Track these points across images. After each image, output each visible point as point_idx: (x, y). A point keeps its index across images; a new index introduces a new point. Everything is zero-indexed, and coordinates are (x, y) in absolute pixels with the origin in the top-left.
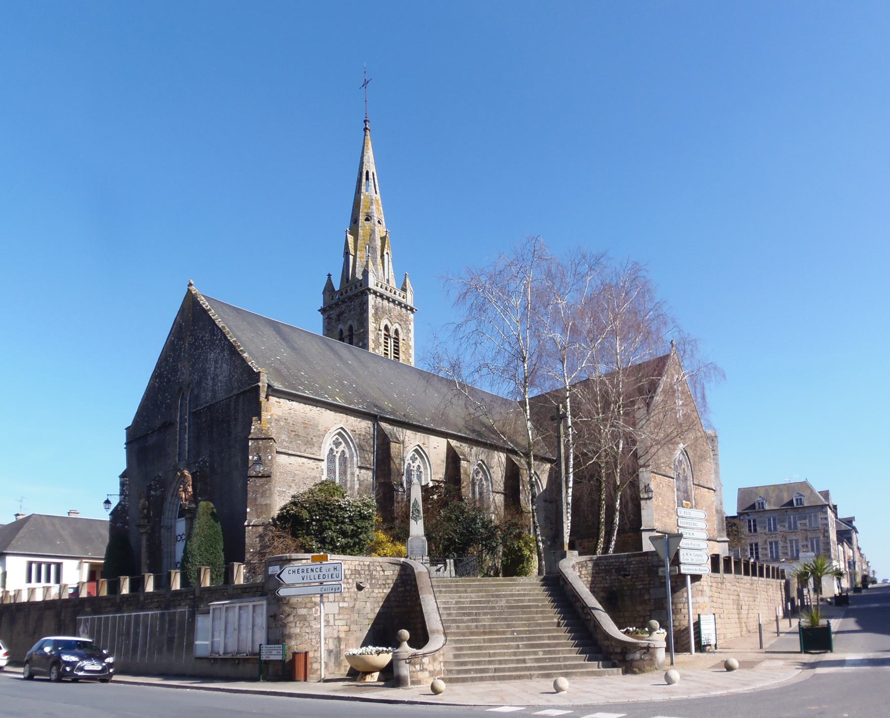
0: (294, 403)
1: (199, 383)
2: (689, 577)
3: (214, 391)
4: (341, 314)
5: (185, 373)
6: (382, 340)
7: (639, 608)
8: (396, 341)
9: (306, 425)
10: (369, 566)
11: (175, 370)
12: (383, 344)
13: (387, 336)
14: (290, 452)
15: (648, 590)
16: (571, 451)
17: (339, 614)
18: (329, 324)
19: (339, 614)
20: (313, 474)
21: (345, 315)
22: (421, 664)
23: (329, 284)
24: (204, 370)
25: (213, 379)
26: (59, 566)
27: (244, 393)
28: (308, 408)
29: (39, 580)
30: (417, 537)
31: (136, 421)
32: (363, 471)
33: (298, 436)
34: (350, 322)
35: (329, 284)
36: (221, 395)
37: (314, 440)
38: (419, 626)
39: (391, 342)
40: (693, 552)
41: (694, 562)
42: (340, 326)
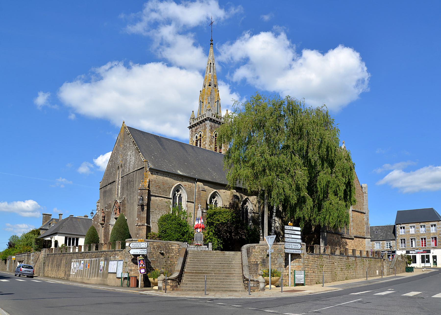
1: (124, 164)
2: (290, 255)
6: (214, 141)
9: (163, 183)
10: (165, 244)
11: (117, 159)
14: (156, 195)
18: (192, 133)
23: (193, 115)
40: (292, 244)
41: (293, 248)
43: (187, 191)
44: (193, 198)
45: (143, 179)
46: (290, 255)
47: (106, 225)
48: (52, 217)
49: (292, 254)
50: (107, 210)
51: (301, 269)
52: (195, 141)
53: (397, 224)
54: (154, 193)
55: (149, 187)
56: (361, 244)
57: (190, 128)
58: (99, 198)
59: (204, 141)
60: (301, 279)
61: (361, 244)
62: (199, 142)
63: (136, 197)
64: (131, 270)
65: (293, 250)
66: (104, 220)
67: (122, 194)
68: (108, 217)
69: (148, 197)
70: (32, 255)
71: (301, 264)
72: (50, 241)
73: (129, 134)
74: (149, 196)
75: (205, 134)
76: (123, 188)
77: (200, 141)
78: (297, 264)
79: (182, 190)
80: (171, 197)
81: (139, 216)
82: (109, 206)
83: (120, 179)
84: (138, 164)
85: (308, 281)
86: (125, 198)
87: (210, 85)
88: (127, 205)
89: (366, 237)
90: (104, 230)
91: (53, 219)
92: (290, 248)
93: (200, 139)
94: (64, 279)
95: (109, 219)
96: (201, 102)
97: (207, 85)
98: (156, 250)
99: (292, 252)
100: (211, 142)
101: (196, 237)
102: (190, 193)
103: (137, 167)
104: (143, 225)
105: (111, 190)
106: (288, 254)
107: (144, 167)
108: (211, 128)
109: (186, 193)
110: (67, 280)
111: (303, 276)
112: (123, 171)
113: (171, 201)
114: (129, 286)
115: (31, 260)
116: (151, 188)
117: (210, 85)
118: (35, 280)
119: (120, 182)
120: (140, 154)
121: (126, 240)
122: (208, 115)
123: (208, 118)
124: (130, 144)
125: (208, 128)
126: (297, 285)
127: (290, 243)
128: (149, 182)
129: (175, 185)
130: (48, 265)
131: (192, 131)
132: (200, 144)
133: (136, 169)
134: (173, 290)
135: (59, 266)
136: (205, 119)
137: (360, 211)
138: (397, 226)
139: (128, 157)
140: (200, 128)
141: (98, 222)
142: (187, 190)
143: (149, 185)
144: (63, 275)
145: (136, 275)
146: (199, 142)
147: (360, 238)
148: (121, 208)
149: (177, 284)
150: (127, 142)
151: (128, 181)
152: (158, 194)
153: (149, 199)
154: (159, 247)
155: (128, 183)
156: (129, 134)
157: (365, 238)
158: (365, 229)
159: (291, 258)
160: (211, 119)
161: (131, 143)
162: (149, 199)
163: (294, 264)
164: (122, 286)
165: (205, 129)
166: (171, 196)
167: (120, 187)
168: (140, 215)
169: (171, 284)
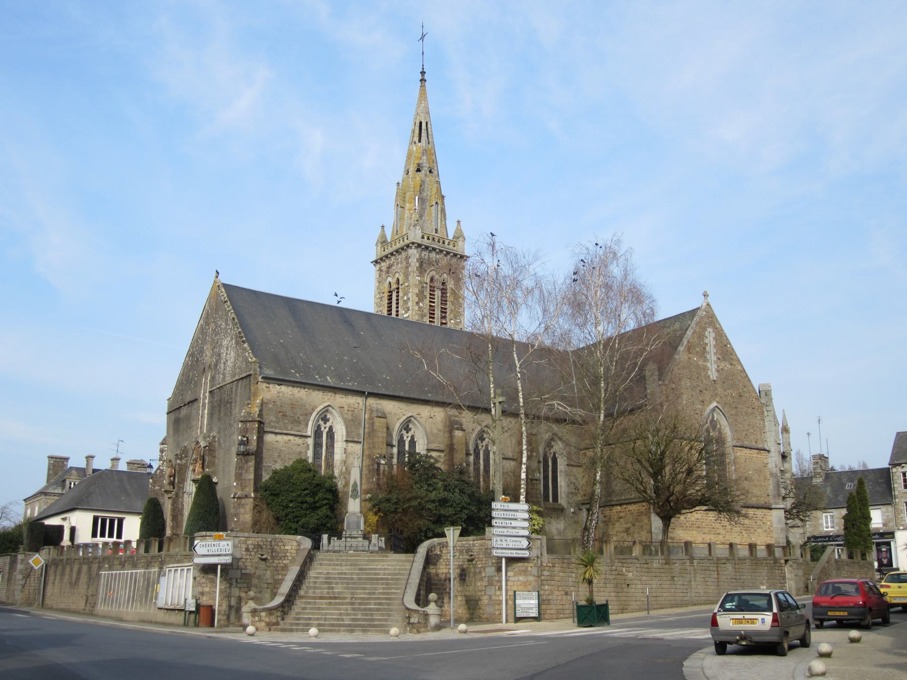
0: (283, 387)
1: (216, 365)
2: (504, 560)
3: (224, 374)
4: (389, 267)
5: (208, 357)
6: (427, 293)
7: (479, 584)
8: (444, 291)
9: (293, 406)
10: (271, 542)
11: (201, 351)
12: (428, 296)
13: (432, 289)
14: (277, 431)
15: (484, 568)
16: (524, 429)
17: (241, 578)
18: (380, 276)
19: (241, 578)
20: (298, 450)
21: (393, 268)
22: (260, 617)
23: (383, 235)
24: (219, 355)
25: (224, 363)
26: (121, 521)
27: (242, 379)
28: (296, 390)
29: (111, 535)
30: (354, 514)
31: (174, 394)
32: (350, 445)
33: (285, 415)
34: (397, 275)
35: (383, 235)
36: (229, 379)
37: (301, 418)
38: (869, 620)
39: (438, 293)
40: (509, 539)
41: (511, 546)
42: (390, 279)
43: (345, 420)
44: (359, 435)
45: (249, 399)
46: (504, 560)
47: (177, 495)
48: (70, 464)
49: (507, 558)
50: (179, 461)
51: (530, 588)
52: (386, 294)
53: (895, 465)
54: (272, 427)
55: (260, 415)
56: (759, 523)
57: (376, 262)
58: (165, 434)
59: (406, 294)
60: (531, 608)
61: (759, 523)
62: (394, 294)
63: (235, 437)
64: (202, 594)
65: (509, 551)
66: (172, 483)
67: (210, 429)
68: (179, 476)
69: (258, 438)
70: (19, 561)
71: (531, 578)
72: (60, 529)
73: (226, 302)
74: (261, 433)
75: (407, 276)
76: (211, 415)
77: (398, 292)
78: (521, 578)
79: (334, 416)
80: (309, 433)
81: (239, 477)
82: (185, 451)
83: (207, 394)
84: (240, 368)
85: (552, 611)
86: (214, 437)
87: (418, 170)
88: (220, 453)
89: (773, 506)
90: (173, 505)
91: (71, 468)
92: (504, 546)
93: (398, 288)
94: (83, 614)
95: (183, 480)
96: (400, 207)
97: (412, 169)
98: (253, 553)
99: (509, 555)
100: (421, 296)
101: (348, 523)
102: (351, 423)
103: (240, 374)
104: (246, 496)
105: (188, 418)
106: (501, 558)
107: (250, 375)
108: (421, 266)
109: (343, 423)
110: (91, 614)
111: (534, 602)
112: (213, 378)
113: (310, 441)
114: (197, 625)
115: (18, 570)
116: (265, 417)
117: (418, 170)
118: (613, 632)
119: (207, 401)
120: (246, 345)
121: (196, 535)
122: (416, 235)
123: (413, 243)
124: (227, 324)
125: (414, 263)
126: (518, 620)
127: (504, 538)
128: (262, 405)
129: (319, 409)
130: (54, 583)
131: (380, 270)
132: (397, 300)
133: (237, 377)
134: (270, 630)
135: (74, 584)
136: (408, 246)
137: (754, 444)
138: (894, 470)
139: (223, 351)
140: (398, 264)
141: (161, 486)
142: (346, 416)
143: (261, 411)
144: (81, 605)
145: (210, 603)
146: (394, 294)
147: (758, 508)
148: (207, 458)
149: (279, 619)
150: (221, 318)
151: (220, 400)
152: (280, 428)
153: (260, 439)
154: (259, 546)
155: (222, 403)
156: (226, 302)
157: (771, 509)
158: (771, 487)
159: (506, 563)
160: (419, 246)
161: (230, 322)
162: (260, 439)
163: (516, 579)
164: (186, 624)
165: (407, 268)
166: (310, 431)
167: (206, 412)
168: (241, 474)
169: (267, 619)
